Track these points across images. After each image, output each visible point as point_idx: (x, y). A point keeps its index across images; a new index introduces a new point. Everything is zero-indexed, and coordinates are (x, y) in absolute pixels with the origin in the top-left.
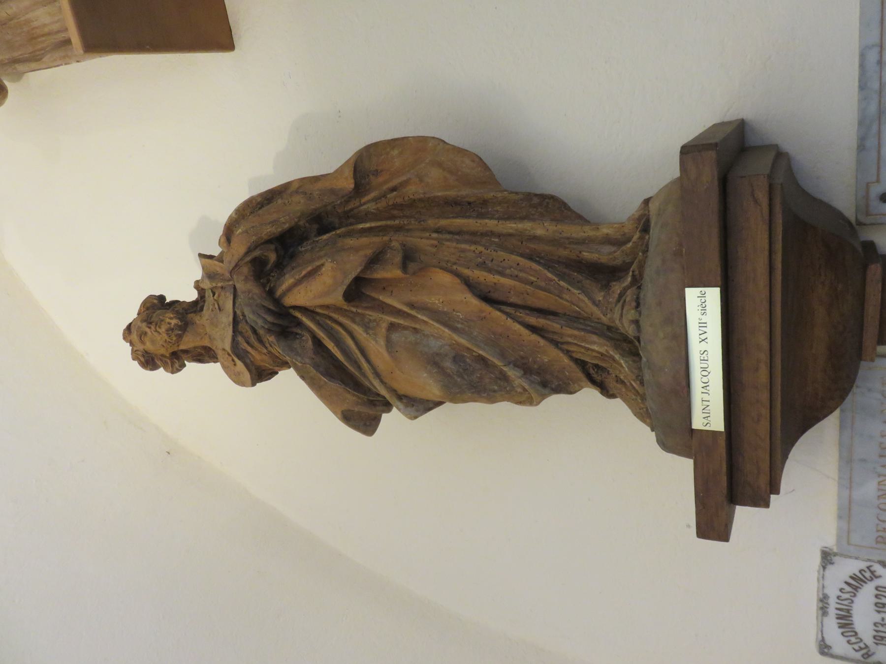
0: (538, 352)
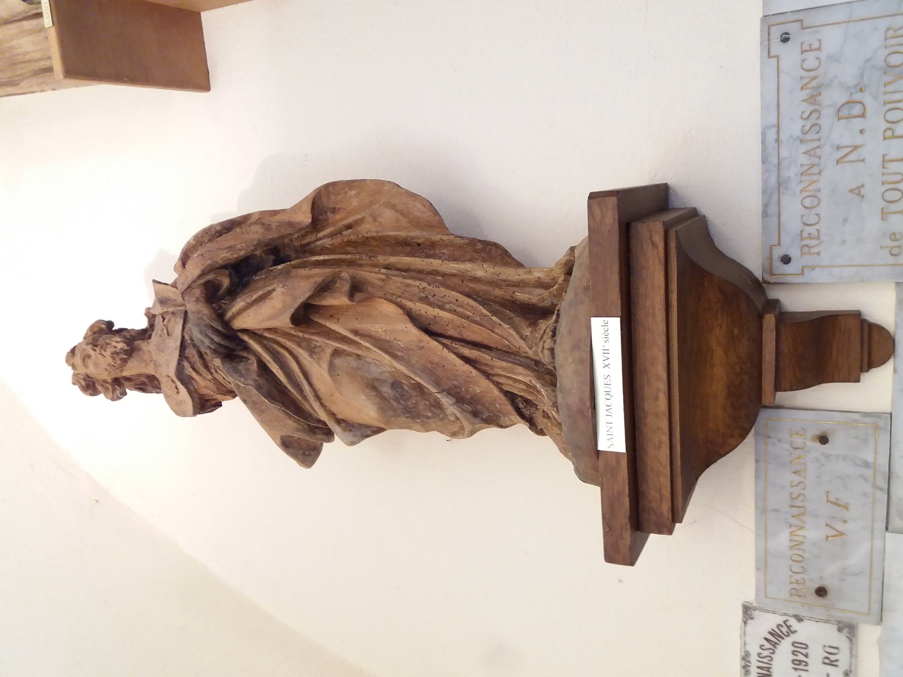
0: (470, 382)
